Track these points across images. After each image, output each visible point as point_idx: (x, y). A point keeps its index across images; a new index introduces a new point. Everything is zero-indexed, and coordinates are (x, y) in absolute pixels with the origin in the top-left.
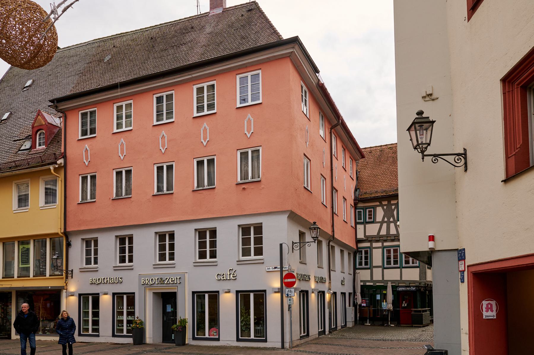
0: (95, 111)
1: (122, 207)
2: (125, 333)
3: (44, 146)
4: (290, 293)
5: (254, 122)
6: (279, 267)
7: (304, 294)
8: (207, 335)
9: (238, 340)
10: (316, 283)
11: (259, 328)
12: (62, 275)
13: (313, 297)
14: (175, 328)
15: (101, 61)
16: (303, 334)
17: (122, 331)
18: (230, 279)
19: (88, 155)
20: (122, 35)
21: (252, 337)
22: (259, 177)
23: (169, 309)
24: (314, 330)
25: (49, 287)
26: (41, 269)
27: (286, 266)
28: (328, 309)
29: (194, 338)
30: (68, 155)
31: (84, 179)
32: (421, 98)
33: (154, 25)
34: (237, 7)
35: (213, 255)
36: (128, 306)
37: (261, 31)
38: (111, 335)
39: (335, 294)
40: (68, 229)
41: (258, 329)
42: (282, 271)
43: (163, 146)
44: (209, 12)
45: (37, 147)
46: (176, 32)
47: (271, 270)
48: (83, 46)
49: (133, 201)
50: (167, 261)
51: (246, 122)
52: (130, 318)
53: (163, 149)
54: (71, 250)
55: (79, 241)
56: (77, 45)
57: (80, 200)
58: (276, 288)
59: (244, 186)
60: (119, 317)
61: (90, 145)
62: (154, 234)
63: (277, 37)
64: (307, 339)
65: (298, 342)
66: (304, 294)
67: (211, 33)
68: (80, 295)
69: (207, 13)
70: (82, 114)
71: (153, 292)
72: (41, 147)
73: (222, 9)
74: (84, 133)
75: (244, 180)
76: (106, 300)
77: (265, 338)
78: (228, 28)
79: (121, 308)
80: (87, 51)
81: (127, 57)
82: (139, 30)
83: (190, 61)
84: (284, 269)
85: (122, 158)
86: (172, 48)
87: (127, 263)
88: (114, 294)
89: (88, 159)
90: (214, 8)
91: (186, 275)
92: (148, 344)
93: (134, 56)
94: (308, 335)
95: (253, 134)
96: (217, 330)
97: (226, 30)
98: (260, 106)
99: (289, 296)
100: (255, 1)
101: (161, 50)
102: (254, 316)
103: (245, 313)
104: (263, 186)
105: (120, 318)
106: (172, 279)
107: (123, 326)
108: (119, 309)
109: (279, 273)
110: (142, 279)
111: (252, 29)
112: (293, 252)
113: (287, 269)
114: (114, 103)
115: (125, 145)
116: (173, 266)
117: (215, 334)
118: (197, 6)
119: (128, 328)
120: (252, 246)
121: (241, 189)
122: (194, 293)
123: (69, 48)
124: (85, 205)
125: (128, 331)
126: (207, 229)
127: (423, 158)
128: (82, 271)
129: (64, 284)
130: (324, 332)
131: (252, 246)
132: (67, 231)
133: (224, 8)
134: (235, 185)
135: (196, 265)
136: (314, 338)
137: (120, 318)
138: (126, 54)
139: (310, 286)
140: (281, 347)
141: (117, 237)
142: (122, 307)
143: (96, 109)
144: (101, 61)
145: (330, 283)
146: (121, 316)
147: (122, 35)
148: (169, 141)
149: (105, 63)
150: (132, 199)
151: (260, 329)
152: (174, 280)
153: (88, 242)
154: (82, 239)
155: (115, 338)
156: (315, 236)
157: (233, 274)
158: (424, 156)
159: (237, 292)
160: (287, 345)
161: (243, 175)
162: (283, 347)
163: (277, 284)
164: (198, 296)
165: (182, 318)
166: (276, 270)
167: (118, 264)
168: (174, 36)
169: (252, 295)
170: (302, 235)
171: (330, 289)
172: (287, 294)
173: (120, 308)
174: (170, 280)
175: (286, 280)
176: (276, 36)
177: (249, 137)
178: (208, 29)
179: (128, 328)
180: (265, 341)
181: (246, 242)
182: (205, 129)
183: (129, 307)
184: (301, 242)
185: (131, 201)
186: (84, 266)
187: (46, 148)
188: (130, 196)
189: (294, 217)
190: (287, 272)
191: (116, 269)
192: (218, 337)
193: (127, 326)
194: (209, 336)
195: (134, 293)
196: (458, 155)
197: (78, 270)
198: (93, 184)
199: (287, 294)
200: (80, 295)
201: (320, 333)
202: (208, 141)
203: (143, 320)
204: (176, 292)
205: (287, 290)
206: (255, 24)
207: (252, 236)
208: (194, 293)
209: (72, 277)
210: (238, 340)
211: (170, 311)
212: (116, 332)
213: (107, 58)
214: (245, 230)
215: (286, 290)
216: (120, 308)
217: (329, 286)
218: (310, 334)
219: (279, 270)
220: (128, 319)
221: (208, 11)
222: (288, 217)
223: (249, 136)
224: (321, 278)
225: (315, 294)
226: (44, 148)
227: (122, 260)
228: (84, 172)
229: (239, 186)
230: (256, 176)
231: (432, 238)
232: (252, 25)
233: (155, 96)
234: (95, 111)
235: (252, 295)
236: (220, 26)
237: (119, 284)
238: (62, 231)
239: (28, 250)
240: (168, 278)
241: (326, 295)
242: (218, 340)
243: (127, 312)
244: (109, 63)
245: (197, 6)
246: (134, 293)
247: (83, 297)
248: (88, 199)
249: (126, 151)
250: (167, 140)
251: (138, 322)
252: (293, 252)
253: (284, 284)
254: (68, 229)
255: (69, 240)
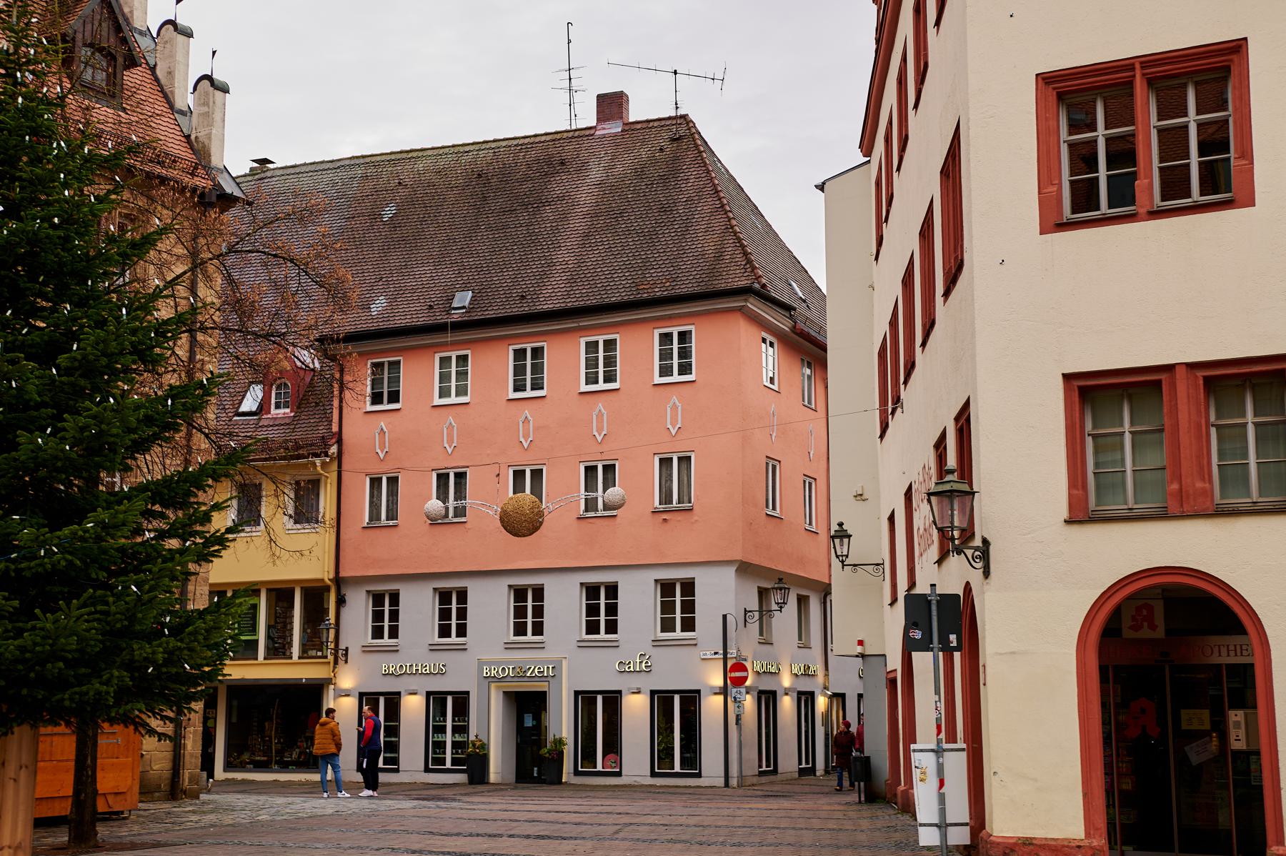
0: (399, 362)
1: (446, 536)
2: (448, 765)
3: (288, 410)
4: (739, 696)
5: (682, 410)
6: (722, 652)
7: (768, 699)
8: (599, 768)
9: (653, 774)
10: (794, 677)
11: (688, 755)
12: (326, 657)
13: (787, 704)
14: (545, 753)
15: (375, 216)
16: (764, 768)
17: (443, 762)
18: (641, 671)
19: (385, 441)
20: (415, 154)
21: (677, 768)
22: (690, 502)
23: (529, 722)
24: (788, 760)
25: (302, 679)
26: (276, 643)
27: (732, 652)
28: (823, 728)
29: (577, 773)
30: (345, 436)
31: (375, 482)
32: (854, 499)
33: (482, 140)
34: (651, 124)
35: (612, 628)
36: (454, 716)
37: (697, 197)
38: (423, 768)
39: (841, 697)
40: (342, 574)
41: (688, 757)
42: (725, 659)
43: (526, 436)
44: (595, 127)
45: (273, 411)
46: (529, 167)
47: (709, 657)
48: (329, 169)
49: (469, 529)
50: (530, 637)
51: (669, 409)
52: (458, 738)
53: (526, 441)
54: (345, 612)
55: (363, 595)
56: (314, 163)
57: (367, 520)
58: (716, 687)
59: (665, 516)
60: (435, 735)
61: (389, 423)
62: (507, 588)
63: (723, 213)
64: (772, 778)
65: (755, 780)
66: (768, 699)
67: (600, 184)
68: (361, 695)
69: (590, 128)
70: (374, 365)
71: (504, 692)
72: (282, 411)
73: (621, 124)
74: (377, 398)
75: (666, 504)
76: (413, 706)
77: (697, 771)
78: (634, 177)
79: (440, 719)
80: (340, 184)
81: (432, 215)
82: (449, 147)
83: (563, 249)
84: (729, 656)
85: (450, 451)
86: (523, 207)
87: (454, 639)
88: (429, 694)
89: (385, 447)
90: (605, 121)
91: (565, 663)
92: (493, 784)
93: (446, 215)
94: (775, 771)
95: (680, 430)
96: (617, 759)
97: (630, 182)
98: (693, 384)
99: (738, 700)
100: (687, 115)
101: (502, 210)
102: (681, 733)
103: (666, 730)
104: (696, 518)
105: (439, 738)
106: (539, 668)
107: (444, 753)
108: (437, 722)
109: (721, 663)
110: (485, 668)
111: (681, 191)
112: (745, 626)
113: (735, 656)
114: (435, 353)
115: (455, 428)
116: (540, 647)
117: (613, 765)
118: (570, 105)
119: (454, 756)
120: (678, 615)
121: (661, 521)
122: (577, 693)
123: (297, 170)
124: (377, 532)
125: (454, 762)
126: (602, 583)
127: (843, 568)
128: (367, 650)
129: (330, 674)
130: (812, 771)
131: (678, 615)
132: (340, 575)
133: (626, 122)
134: (651, 514)
135: (582, 645)
136: (790, 778)
137: (439, 738)
138: (428, 208)
139: (780, 683)
140: (723, 786)
141: (435, 589)
142: (442, 719)
143: (401, 358)
144: (375, 219)
145: (827, 675)
146: (440, 735)
147: (415, 154)
148: (536, 429)
149: (384, 223)
150: (467, 526)
151: (691, 757)
152: (544, 671)
153: (378, 599)
154: (367, 591)
155: (431, 774)
156: (782, 601)
157: (647, 663)
158: (843, 565)
159: (653, 693)
160: (734, 782)
161: (664, 496)
162: (727, 784)
163: (718, 681)
164: (585, 699)
165: (557, 737)
166: (717, 656)
167: (437, 640)
168: (526, 179)
169: (677, 699)
170: (763, 593)
171: (826, 688)
172: (735, 697)
173: (438, 719)
174: (536, 670)
175: (733, 675)
176: (720, 210)
177: (674, 434)
178: (594, 173)
179: (454, 756)
180: (699, 775)
181: (667, 607)
182: (600, 415)
183: (457, 719)
184: (764, 609)
185: (466, 528)
186: (370, 640)
187: (292, 414)
188: (463, 520)
189: (745, 569)
190: (734, 661)
191: (434, 649)
192: (618, 770)
193: (452, 754)
194: (603, 768)
195: (468, 693)
196: (878, 565)
197: (359, 649)
198: (393, 493)
199: (735, 697)
200: (361, 695)
201: (802, 772)
202: (605, 435)
203: (486, 742)
204: (546, 692)
205: (735, 690)
206: (686, 177)
207: (678, 599)
208: (577, 693)
209: (346, 662)
210: (653, 774)
211: (530, 725)
212: (434, 760)
213: (389, 212)
214: (667, 588)
215: (733, 691)
216: (438, 719)
217: (825, 682)
218: (780, 770)
219: (722, 656)
220: (454, 740)
221: (594, 124)
222: (736, 571)
223: (674, 432)
224: (806, 667)
225: (753, 697)
226: (287, 413)
227: (444, 632)
228: (376, 469)
229: (657, 516)
230: (686, 499)
231: (861, 643)
232: (680, 179)
233: (511, 348)
234: (399, 362)
235: (677, 699)
236: (619, 169)
237: (438, 676)
238: (331, 576)
239: (255, 607)
240: (533, 667)
241: (781, 701)
242: (619, 774)
243: (453, 726)
244: (394, 223)
245: (570, 105)
246: (468, 693)
247: (370, 699)
248: (382, 520)
249: (457, 439)
250: (533, 427)
251: (478, 743)
252: (745, 626)
253: (730, 680)
254: (342, 574)
255: (343, 592)
